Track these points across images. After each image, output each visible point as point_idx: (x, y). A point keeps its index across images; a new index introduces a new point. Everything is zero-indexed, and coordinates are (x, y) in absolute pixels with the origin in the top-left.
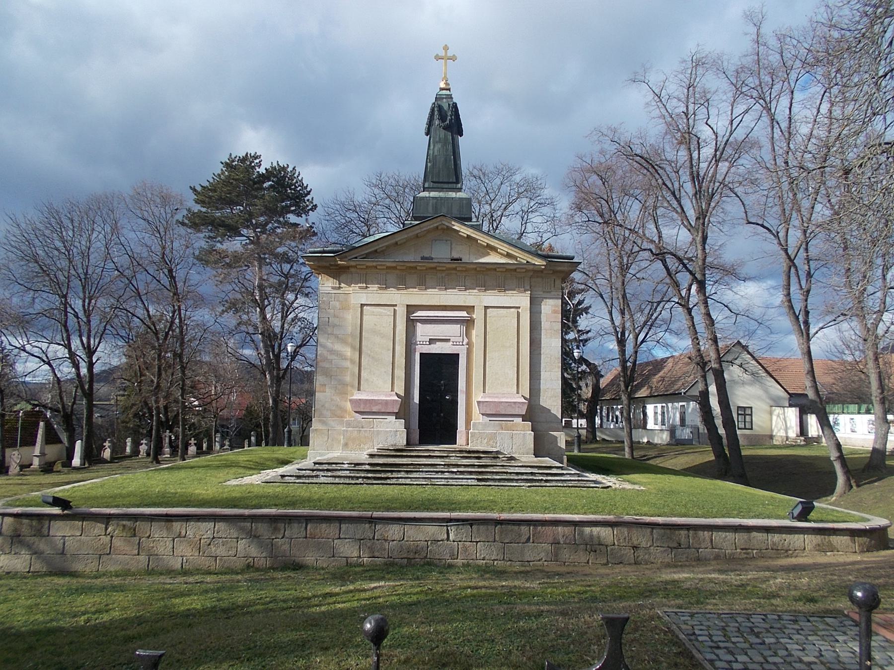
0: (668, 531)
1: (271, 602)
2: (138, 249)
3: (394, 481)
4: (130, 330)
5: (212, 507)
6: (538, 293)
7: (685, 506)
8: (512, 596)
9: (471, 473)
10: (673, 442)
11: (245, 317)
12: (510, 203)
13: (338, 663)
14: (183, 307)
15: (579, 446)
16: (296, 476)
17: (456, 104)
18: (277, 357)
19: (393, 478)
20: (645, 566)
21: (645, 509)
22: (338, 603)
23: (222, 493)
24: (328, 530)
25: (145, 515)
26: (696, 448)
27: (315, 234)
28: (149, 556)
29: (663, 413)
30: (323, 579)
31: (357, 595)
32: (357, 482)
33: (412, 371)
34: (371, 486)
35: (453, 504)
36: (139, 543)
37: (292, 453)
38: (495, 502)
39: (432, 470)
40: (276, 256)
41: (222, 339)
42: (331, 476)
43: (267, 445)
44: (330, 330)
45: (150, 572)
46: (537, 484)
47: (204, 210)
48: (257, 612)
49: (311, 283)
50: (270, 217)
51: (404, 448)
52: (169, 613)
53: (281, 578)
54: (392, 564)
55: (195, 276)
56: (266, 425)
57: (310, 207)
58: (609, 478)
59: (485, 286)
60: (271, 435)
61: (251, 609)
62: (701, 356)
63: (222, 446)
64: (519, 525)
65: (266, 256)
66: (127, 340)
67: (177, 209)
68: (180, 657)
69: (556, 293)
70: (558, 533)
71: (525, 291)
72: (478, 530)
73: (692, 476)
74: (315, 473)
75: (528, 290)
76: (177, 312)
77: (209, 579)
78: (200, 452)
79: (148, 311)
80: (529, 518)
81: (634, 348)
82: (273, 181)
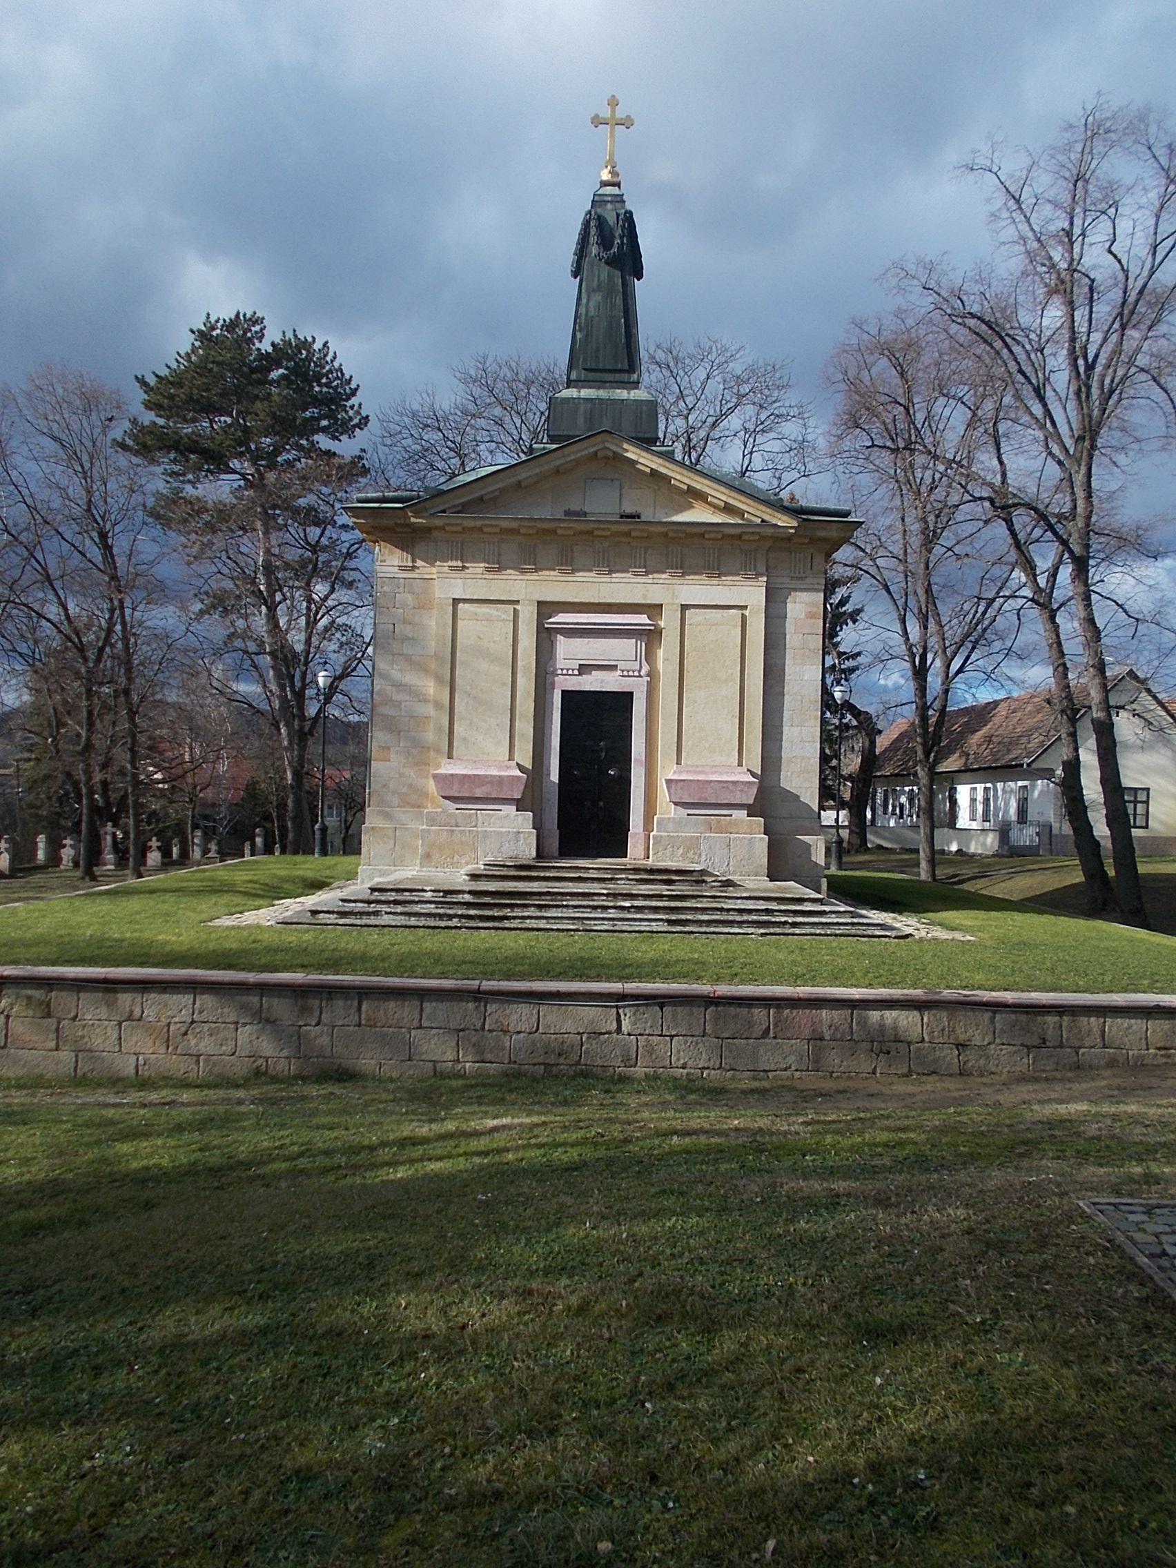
0: (1023, 1017)
1: (301, 1155)
2: (43, 494)
3: (515, 924)
4: (36, 642)
5: (188, 966)
6: (783, 581)
7: (1052, 970)
8: (762, 1151)
9: (656, 909)
10: (1005, 851)
11: (240, 623)
12: (724, 415)
13: (444, 1311)
14: (128, 603)
15: (840, 858)
16: (337, 913)
17: (631, 213)
18: (300, 696)
19: (514, 918)
20: (979, 1080)
21: (979, 977)
22: (430, 1160)
23: (206, 941)
24: (405, 1011)
25: (66, 979)
26: (1048, 861)
27: (365, 471)
28: (77, 1051)
29: (986, 801)
30: (392, 1101)
31: (463, 1143)
32: (450, 924)
33: (547, 723)
34: (475, 933)
35: (626, 966)
36: (57, 1030)
37: (329, 868)
38: (704, 963)
39: (585, 903)
40: (296, 511)
41: (200, 662)
42: (401, 914)
43: (283, 852)
44: (395, 646)
45: (80, 1081)
46: (778, 930)
47: (161, 421)
48: (277, 1176)
49: (361, 561)
50: (283, 437)
51: (532, 863)
52: (110, 1174)
53: (319, 1096)
54: (518, 1075)
55: (147, 547)
56: (281, 818)
57: (356, 421)
58: (899, 918)
59: (684, 568)
60: (291, 836)
61: (267, 1169)
62: (1069, 697)
63: (206, 851)
64: (750, 1006)
65: (278, 512)
66: (30, 660)
67: (110, 420)
68: (126, 1283)
69: (816, 581)
70: (820, 1021)
71: (758, 575)
72: (674, 1015)
73: (1034, 912)
74: (373, 908)
75: (762, 575)
76: (117, 612)
77: (185, 1096)
78: (168, 863)
79: (66, 609)
80: (770, 994)
81: (943, 684)
82: (286, 368)
